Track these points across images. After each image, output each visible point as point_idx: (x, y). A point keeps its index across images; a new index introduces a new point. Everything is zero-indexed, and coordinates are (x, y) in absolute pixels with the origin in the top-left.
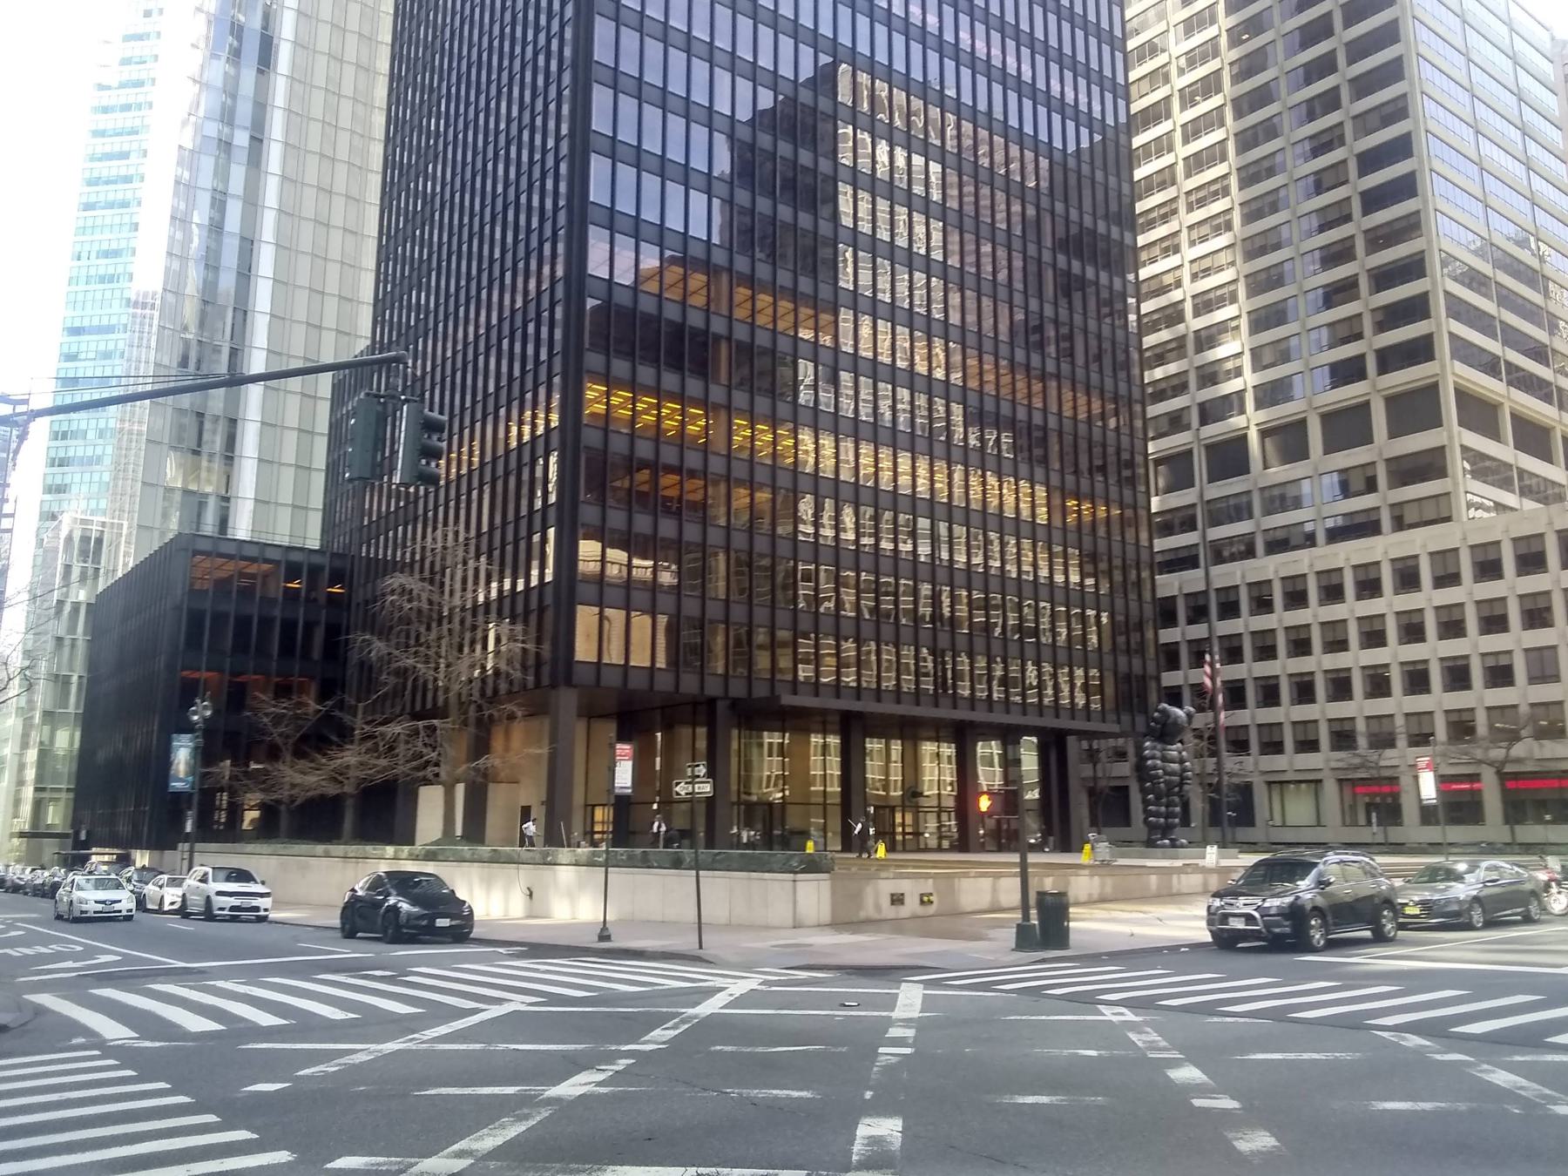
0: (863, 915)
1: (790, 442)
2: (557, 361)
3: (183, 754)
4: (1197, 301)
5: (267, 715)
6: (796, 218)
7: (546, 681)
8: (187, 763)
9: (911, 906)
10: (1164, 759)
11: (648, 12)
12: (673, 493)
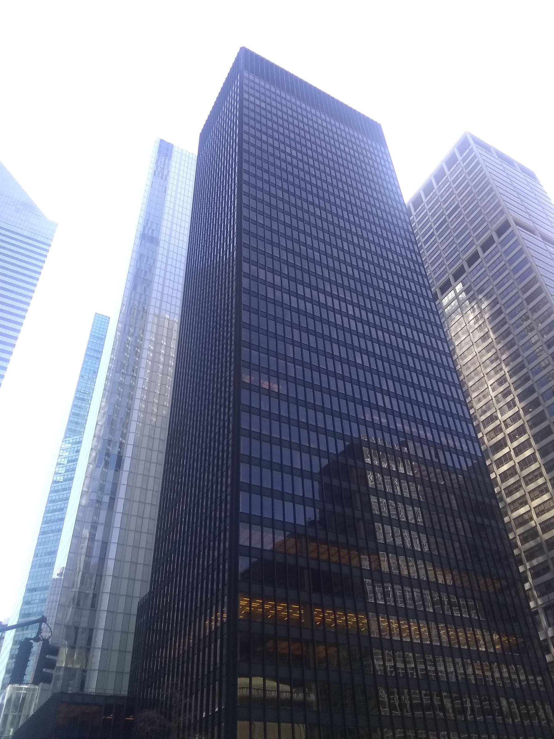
2: (226, 588)
4: (542, 526)
11: (292, 441)
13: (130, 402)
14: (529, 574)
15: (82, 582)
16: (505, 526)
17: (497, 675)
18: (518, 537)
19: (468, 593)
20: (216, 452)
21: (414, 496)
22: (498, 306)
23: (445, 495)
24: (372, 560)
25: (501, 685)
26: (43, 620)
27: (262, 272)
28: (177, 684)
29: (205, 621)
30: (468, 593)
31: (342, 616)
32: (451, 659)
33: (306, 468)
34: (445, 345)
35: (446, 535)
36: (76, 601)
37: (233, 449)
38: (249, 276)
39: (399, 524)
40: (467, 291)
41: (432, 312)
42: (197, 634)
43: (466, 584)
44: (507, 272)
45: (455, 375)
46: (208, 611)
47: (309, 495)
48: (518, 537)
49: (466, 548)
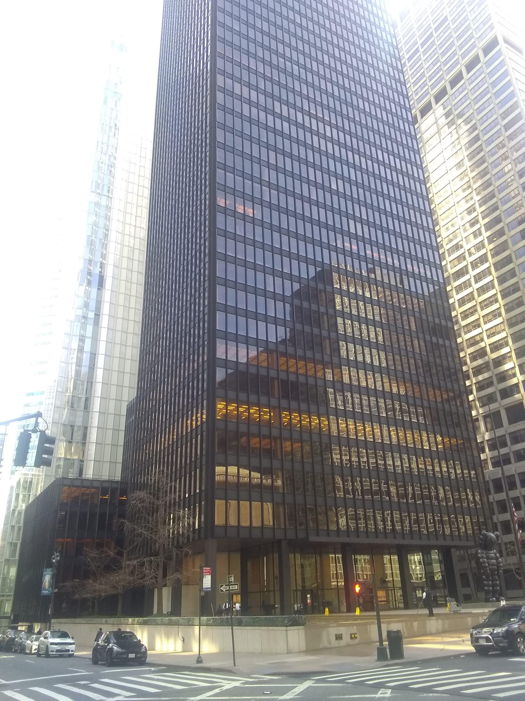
0: (321, 646)
1: (344, 425)
2: (205, 394)
3: (47, 579)
5: (89, 557)
6: (312, 330)
7: (202, 536)
8: (49, 582)
9: (346, 639)
10: (488, 558)
12: (258, 445)
13: (108, 223)
14: (474, 388)
15: (75, 388)
16: (457, 347)
17: (437, 469)
18: (468, 356)
19: (418, 402)
20: (193, 274)
21: (377, 318)
22: (476, 132)
23: (405, 318)
24: (335, 373)
25: (440, 476)
26: (39, 415)
27: (237, 86)
28: (163, 471)
29: (187, 420)
30: (418, 402)
31: (307, 418)
32: (398, 455)
33: (279, 291)
34: (420, 171)
35: (403, 353)
36: (70, 403)
37: (209, 272)
38: (224, 90)
39: (362, 342)
40: (447, 115)
41: (411, 136)
42: (180, 432)
43: (417, 395)
44: (489, 95)
45: (426, 203)
46: (190, 412)
47: (280, 316)
48: (468, 356)
49: (420, 365)
